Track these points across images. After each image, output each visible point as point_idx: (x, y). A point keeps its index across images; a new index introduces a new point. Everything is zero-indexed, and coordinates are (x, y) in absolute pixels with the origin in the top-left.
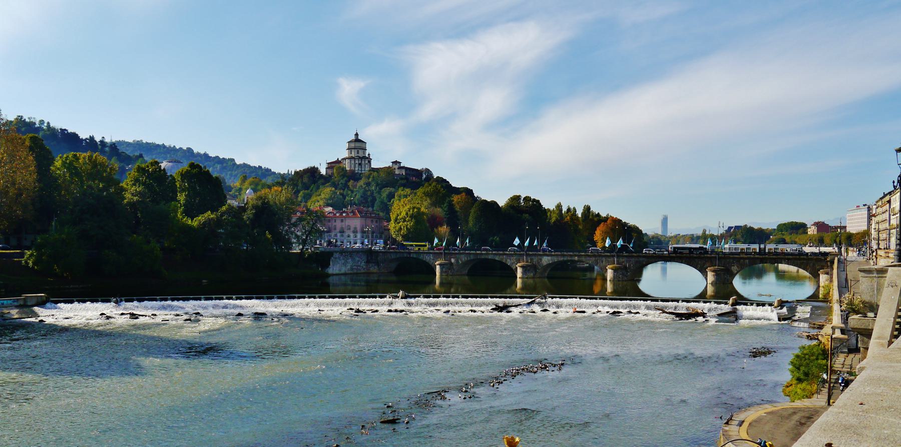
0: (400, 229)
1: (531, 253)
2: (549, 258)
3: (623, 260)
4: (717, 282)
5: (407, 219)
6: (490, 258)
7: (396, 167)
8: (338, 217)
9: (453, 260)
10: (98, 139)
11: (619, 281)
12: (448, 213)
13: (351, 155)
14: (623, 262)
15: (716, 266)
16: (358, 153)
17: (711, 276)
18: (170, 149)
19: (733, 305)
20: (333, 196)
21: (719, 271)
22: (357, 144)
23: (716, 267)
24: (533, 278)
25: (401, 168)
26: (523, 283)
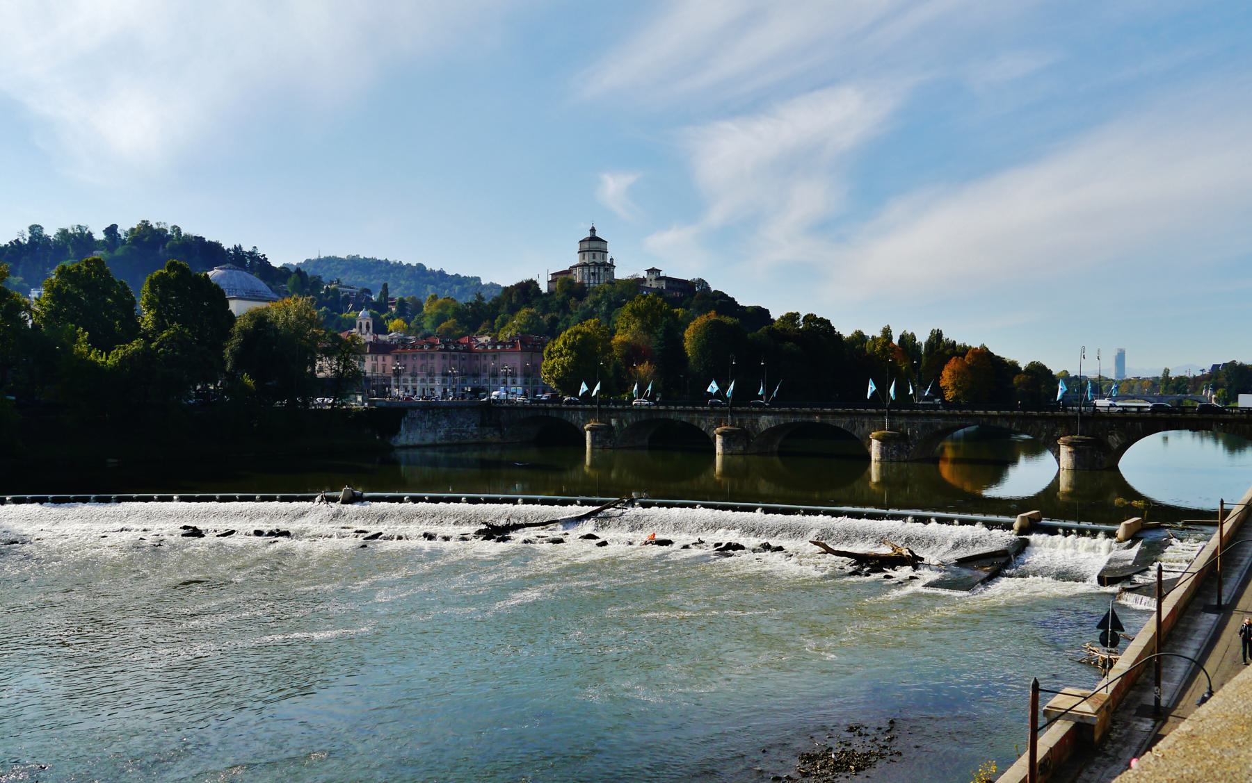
0: (554, 368)
1: (739, 409)
2: (771, 418)
3: (901, 422)
4: (1078, 467)
5: (564, 352)
6: (672, 418)
7: (653, 277)
8: (489, 351)
9: (613, 422)
10: (51, 232)
11: (891, 461)
12: (663, 342)
13: (584, 261)
14: (901, 426)
15: (1076, 435)
16: (594, 257)
17: (1064, 451)
18: (394, 266)
19: (1022, 531)
20: (531, 322)
21: (1079, 444)
22: (594, 244)
23: (1076, 437)
24: (743, 454)
25: (659, 279)
26: (724, 462)
